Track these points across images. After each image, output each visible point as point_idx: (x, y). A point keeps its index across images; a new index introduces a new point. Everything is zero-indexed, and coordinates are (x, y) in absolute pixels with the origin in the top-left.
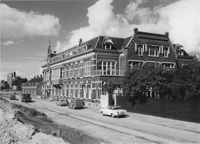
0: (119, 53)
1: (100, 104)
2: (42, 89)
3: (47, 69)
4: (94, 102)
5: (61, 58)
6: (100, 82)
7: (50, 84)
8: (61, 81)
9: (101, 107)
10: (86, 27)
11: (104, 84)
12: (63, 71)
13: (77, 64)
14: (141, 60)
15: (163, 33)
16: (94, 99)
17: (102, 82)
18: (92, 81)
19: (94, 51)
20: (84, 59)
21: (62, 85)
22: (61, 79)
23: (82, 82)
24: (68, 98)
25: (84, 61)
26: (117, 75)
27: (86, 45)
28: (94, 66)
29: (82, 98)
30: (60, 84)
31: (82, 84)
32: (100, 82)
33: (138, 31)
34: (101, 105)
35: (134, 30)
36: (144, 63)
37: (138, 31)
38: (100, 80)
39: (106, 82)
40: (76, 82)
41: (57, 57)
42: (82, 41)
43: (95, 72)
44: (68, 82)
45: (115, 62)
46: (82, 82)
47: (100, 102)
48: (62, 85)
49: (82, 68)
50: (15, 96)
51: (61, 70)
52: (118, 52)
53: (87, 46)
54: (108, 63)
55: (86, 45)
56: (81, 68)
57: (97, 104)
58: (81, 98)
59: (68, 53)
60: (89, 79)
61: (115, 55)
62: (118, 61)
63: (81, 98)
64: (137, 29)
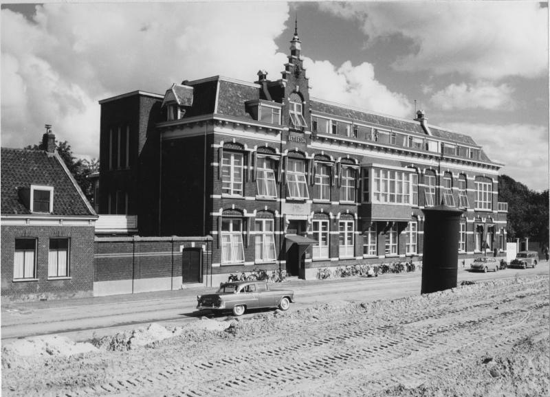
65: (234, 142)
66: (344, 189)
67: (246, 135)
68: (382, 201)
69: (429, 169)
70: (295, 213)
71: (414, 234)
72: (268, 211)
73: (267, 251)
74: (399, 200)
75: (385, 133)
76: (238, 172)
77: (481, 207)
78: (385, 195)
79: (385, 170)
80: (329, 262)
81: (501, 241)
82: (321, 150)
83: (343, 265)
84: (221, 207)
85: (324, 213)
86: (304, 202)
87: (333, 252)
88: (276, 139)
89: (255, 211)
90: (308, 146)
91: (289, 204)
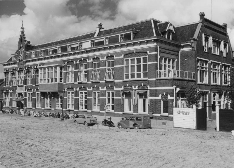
0: (180, 47)
1: (171, 121)
2: (4, 99)
3: (17, 68)
4: (156, 119)
5: (58, 51)
6: (172, 88)
7: (26, 91)
8: (61, 86)
9: (175, 126)
10: (12, 16)
11: (177, 91)
12: (63, 71)
13: (92, 62)
14: (207, 59)
15: (221, 24)
16: (65, 111)
17: (175, 88)
18: (88, 89)
19: (155, 41)
20: (126, 53)
21: (62, 92)
22: (61, 83)
23: (90, 88)
24: (79, 112)
25: (124, 55)
26: (181, 78)
27: (131, 32)
28: (156, 63)
29: (77, 110)
30: (60, 91)
31: (122, 90)
32: (172, 88)
33: (205, 17)
34: (174, 123)
35: (200, 15)
36: (209, 63)
37: (205, 17)
38: (173, 86)
39: (180, 89)
40: (11, 91)
41: (48, 50)
42: (103, 27)
43: (157, 72)
44: (35, 90)
45: (175, 59)
46: (90, 88)
47: (172, 119)
48: (62, 92)
49: (91, 70)
50: (30, 112)
51: (61, 69)
52: (180, 44)
53: (133, 33)
54: (165, 59)
55: (131, 32)
56: (101, 68)
57: (164, 121)
58: (134, 114)
59: (78, 44)
60: (141, 83)
61: (175, 48)
62: (178, 59)
63: (134, 114)
64: (204, 14)
65: (110, 55)
66: (9, 81)
67: (122, 50)
68: (42, 83)
69: (69, 62)
70: (21, 90)
71: (72, 98)
72: (84, 88)
73: (39, 105)
74: (52, 81)
75: (56, 49)
76: (160, 63)
77: (186, 72)
78: (45, 80)
79: (52, 67)
80: (32, 109)
81: (135, 101)
82: (29, 65)
83: (37, 111)
84: (91, 87)
85: (71, 88)
86: (22, 86)
87: (34, 105)
88: (16, 65)
89: (92, 88)
90: (25, 65)
91: (19, 87)
